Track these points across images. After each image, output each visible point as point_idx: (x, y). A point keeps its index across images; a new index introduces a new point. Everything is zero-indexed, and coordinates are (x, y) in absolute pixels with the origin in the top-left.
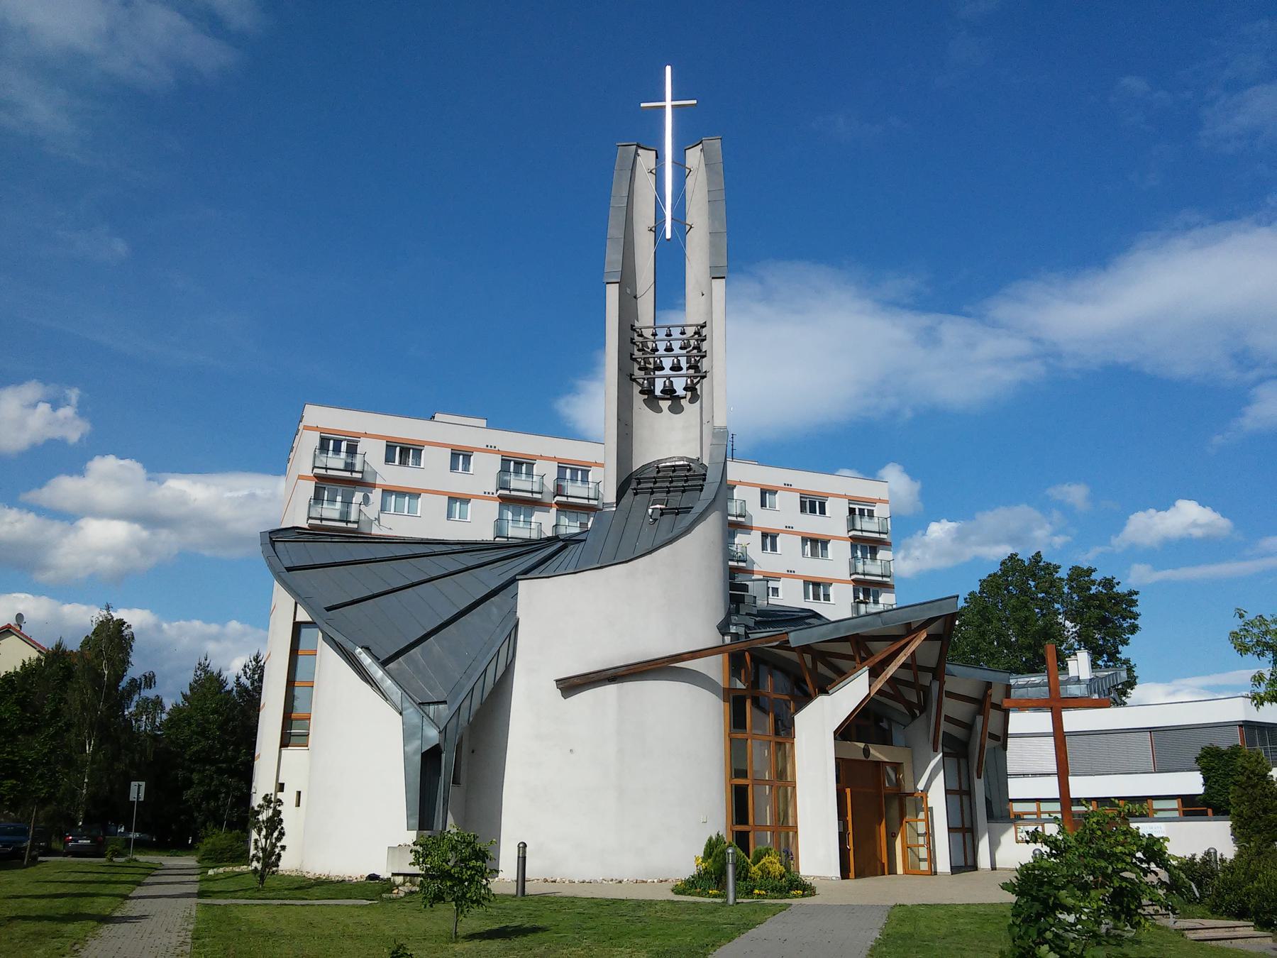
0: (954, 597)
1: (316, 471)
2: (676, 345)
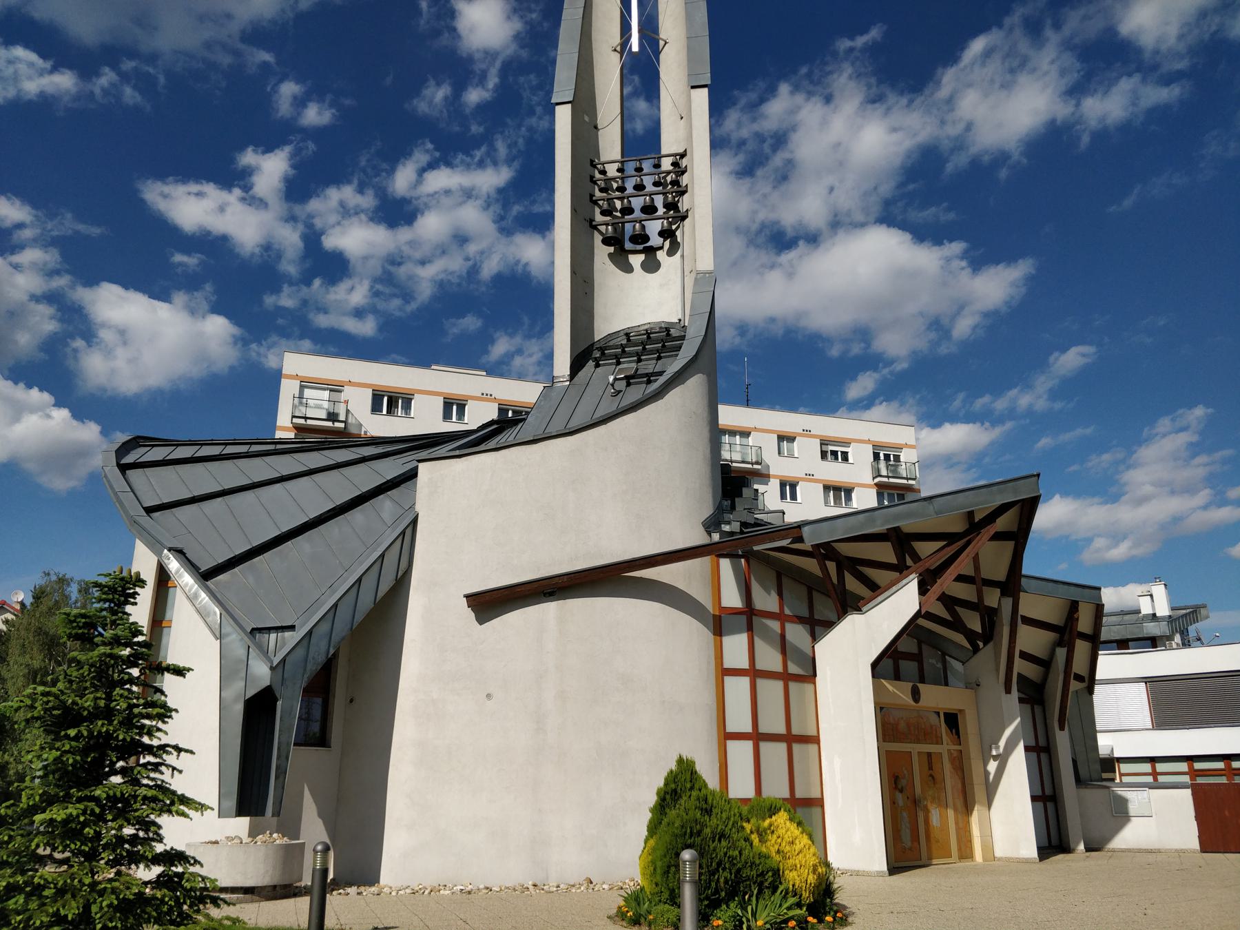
0: (1034, 476)
1: (295, 420)
2: (648, 181)
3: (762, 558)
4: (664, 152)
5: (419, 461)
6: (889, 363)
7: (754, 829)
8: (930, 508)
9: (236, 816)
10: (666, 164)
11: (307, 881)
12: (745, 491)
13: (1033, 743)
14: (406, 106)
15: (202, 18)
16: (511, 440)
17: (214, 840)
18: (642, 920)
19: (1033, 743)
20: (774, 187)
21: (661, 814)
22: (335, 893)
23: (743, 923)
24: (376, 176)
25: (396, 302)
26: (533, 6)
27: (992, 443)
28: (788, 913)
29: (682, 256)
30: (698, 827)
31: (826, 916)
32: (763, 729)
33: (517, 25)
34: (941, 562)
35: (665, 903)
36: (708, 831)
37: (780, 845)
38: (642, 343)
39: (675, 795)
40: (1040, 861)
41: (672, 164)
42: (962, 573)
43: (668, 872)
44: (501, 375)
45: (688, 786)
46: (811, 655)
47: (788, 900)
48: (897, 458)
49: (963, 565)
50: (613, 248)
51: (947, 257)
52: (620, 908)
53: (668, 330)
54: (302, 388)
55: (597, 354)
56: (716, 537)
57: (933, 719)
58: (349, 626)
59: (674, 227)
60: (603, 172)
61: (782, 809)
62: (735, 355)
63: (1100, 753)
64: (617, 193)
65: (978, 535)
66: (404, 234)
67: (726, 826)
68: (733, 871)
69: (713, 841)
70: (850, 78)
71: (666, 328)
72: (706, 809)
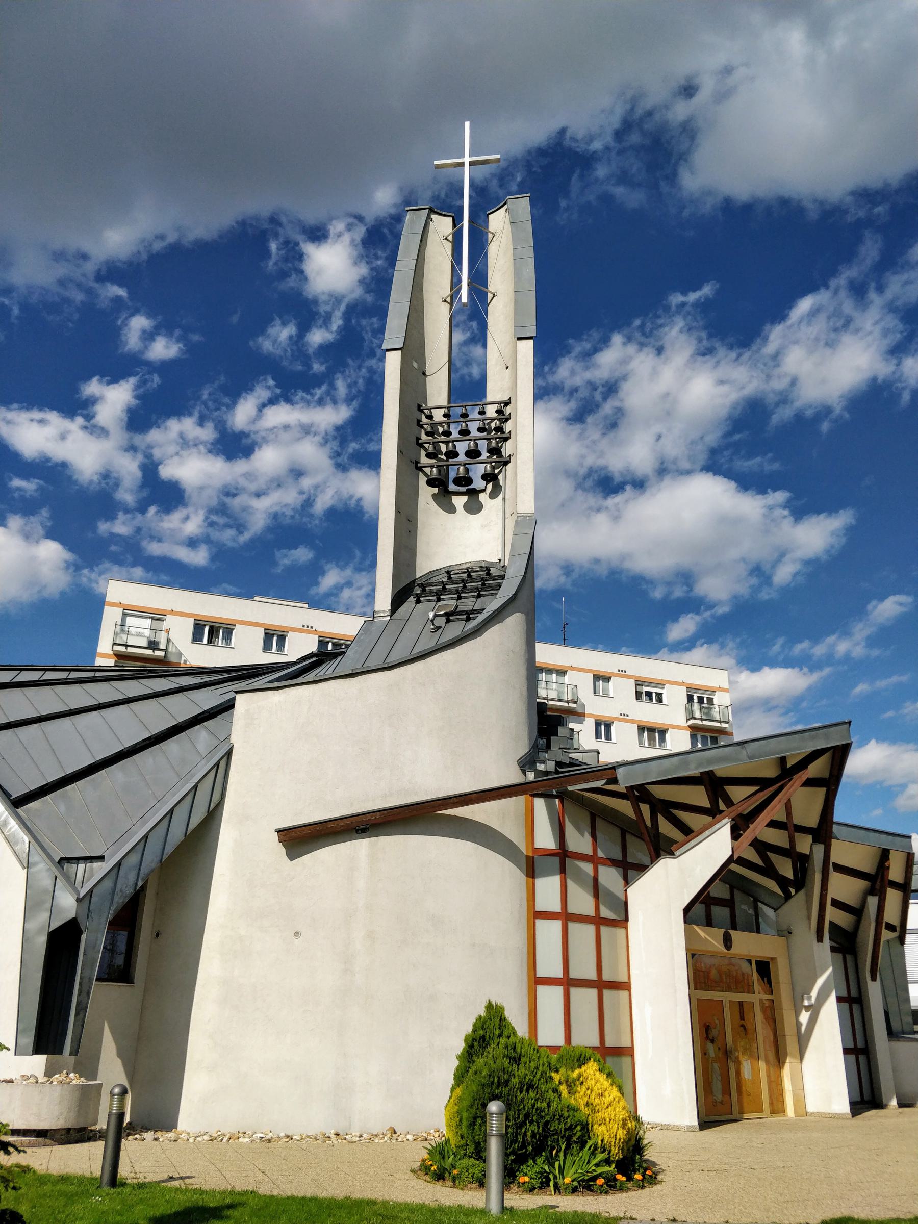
0: (845, 723)
1: (116, 648)
2: (473, 427)
3: (577, 799)
4: (489, 399)
5: (237, 692)
6: (711, 606)
7: (563, 1080)
8: (743, 753)
9: (32, 1055)
10: (491, 411)
11: (102, 1124)
12: (561, 730)
13: (845, 994)
14: (251, 343)
15: (59, 256)
16: (329, 673)
17: (8, 1079)
18: (447, 1174)
19: (845, 994)
20: (604, 434)
21: (468, 1062)
22: (130, 1138)
23: (550, 1180)
24: (217, 409)
25: (230, 533)
26: (380, 253)
27: (809, 689)
28: (597, 1169)
29: (504, 499)
30: (506, 1076)
31: (635, 1174)
32: (573, 974)
33: (363, 270)
34: (752, 807)
35: (470, 1157)
36: (515, 1081)
37: (589, 1098)
38: (463, 581)
39: (484, 1041)
40: (853, 1117)
41: (497, 412)
42: (775, 818)
43: (474, 1124)
44: (329, 608)
45: (497, 1032)
46: (624, 899)
47: (597, 1155)
48: (710, 701)
49: (775, 811)
50: (437, 489)
51: (769, 506)
52: (424, 1161)
53: (488, 569)
54: (125, 615)
55: (418, 590)
56: (531, 776)
57: (745, 967)
58: (159, 859)
59: (496, 471)
60: (430, 417)
61: (592, 1060)
62: (557, 593)
63: (912, 1004)
64: (443, 437)
65: (790, 781)
66: (241, 466)
67: (534, 1077)
68: (541, 1124)
69: (521, 1092)
70: (681, 331)
71: (486, 567)
72: (514, 1058)
